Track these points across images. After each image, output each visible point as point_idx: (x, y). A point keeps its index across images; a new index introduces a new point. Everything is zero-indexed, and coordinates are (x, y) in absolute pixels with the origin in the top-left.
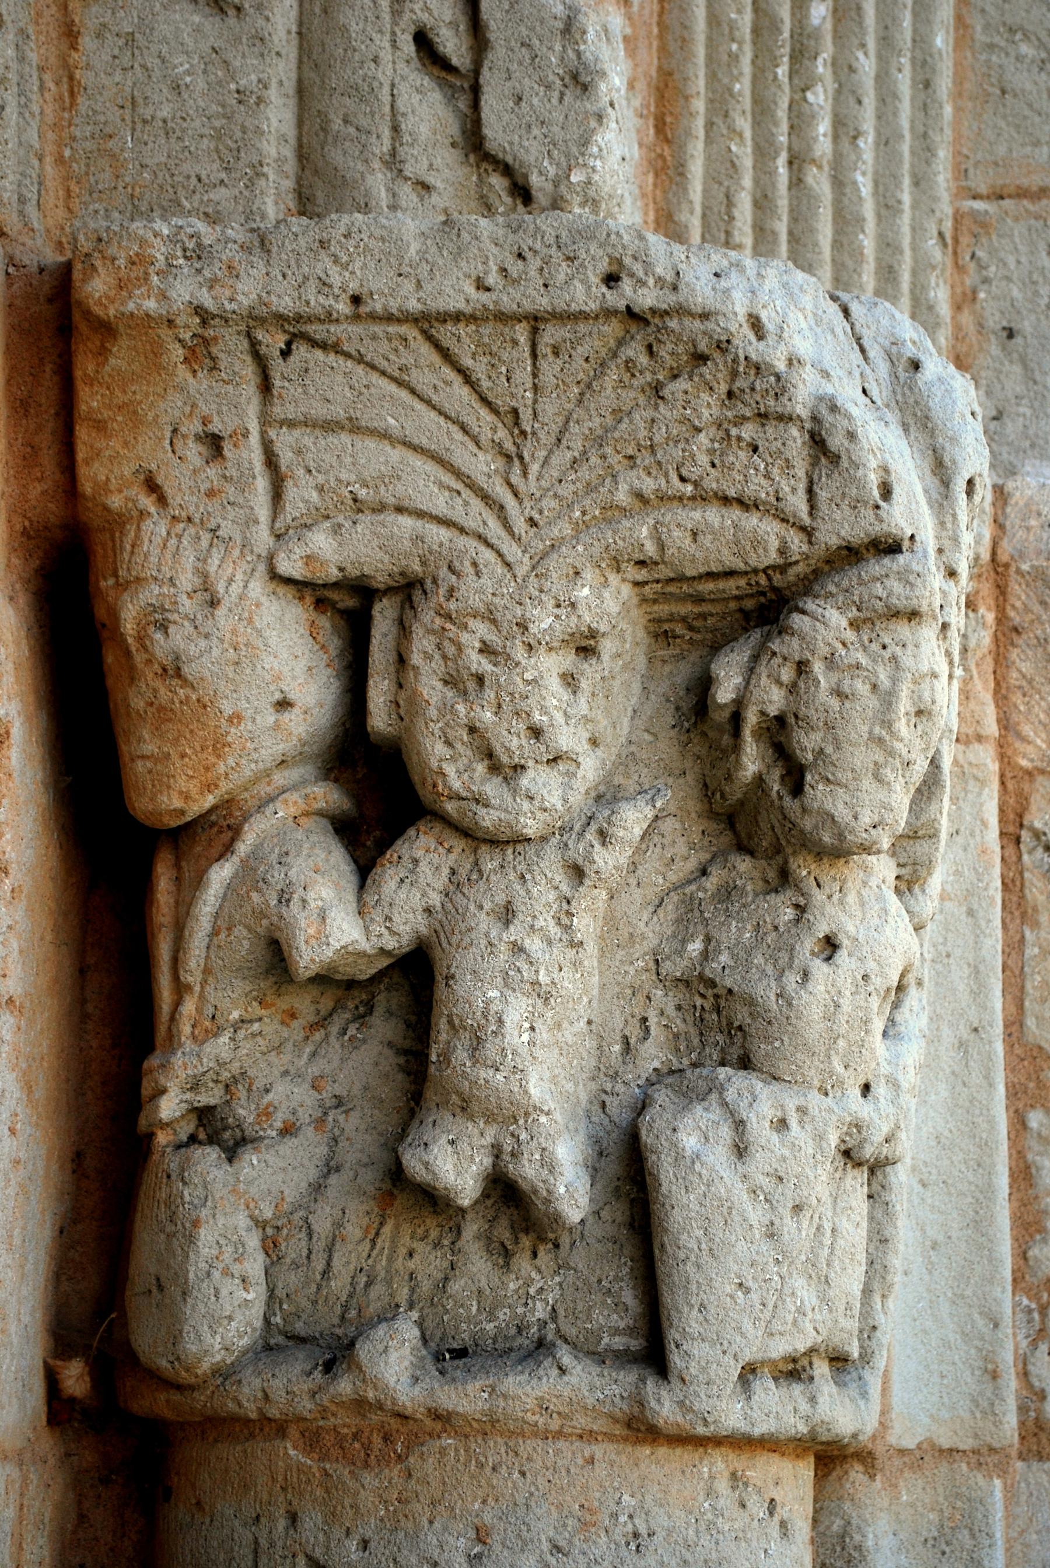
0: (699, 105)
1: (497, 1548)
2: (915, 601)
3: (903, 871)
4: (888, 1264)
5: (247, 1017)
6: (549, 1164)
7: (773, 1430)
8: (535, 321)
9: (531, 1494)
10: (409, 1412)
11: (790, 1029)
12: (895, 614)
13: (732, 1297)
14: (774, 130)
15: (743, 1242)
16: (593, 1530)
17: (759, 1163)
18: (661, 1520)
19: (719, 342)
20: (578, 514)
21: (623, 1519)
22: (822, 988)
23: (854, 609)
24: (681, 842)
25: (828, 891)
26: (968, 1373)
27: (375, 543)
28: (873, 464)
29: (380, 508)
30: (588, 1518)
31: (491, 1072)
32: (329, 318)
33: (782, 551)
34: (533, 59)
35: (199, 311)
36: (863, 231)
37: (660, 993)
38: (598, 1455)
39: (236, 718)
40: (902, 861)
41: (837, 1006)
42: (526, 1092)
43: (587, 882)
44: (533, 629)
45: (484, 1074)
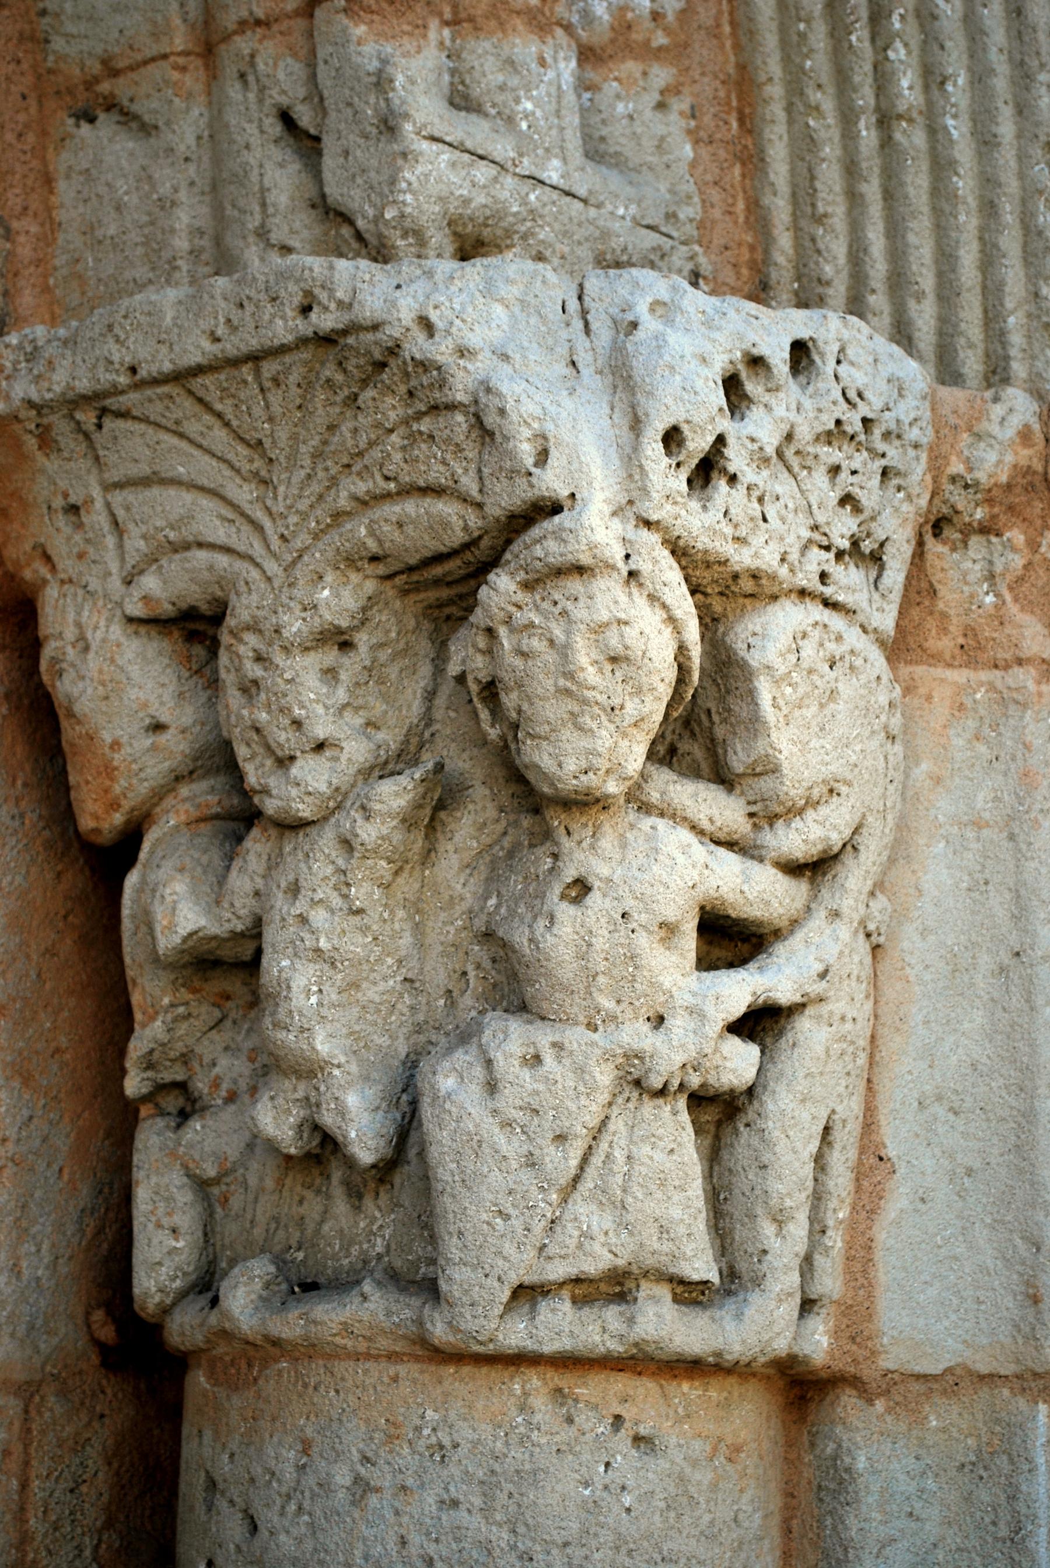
0: (776, 91)
1: (316, 1457)
2: (570, 557)
3: (753, 809)
4: (770, 1190)
5: (177, 1002)
6: (342, 1112)
7: (568, 1348)
8: (255, 358)
9: (344, 1410)
10: (251, 1339)
11: (543, 970)
12: (560, 572)
13: (488, 1223)
14: (854, 96)
15: (498, 1173)
16: (397, 1442)
17: (509, 1100)
18: (465, 1433)
19: (388, 348)
20: (313, 524)
21: (426, 1432)
22: (569, 930)
23: (522, 573)
24: (489, 805)
25: (576, 837)
26: (1010, 1298)
27: (186, 577)
28: (527, 433)
29: (187, 546)
30: (392, 1430)
31: (284, 1033)
32: (116, 391)
33: (466, 528)
34: (355, 115)
35: (30, 404)
36: (957, 174)
37: (477, 948)
38: (402, 1374)
39: (116, 745)
40: (751, 798)
41: (590, 945)
42: (313, 1048)
43: (357, 854)
44: (285, 633)
45: (281, 1035)
